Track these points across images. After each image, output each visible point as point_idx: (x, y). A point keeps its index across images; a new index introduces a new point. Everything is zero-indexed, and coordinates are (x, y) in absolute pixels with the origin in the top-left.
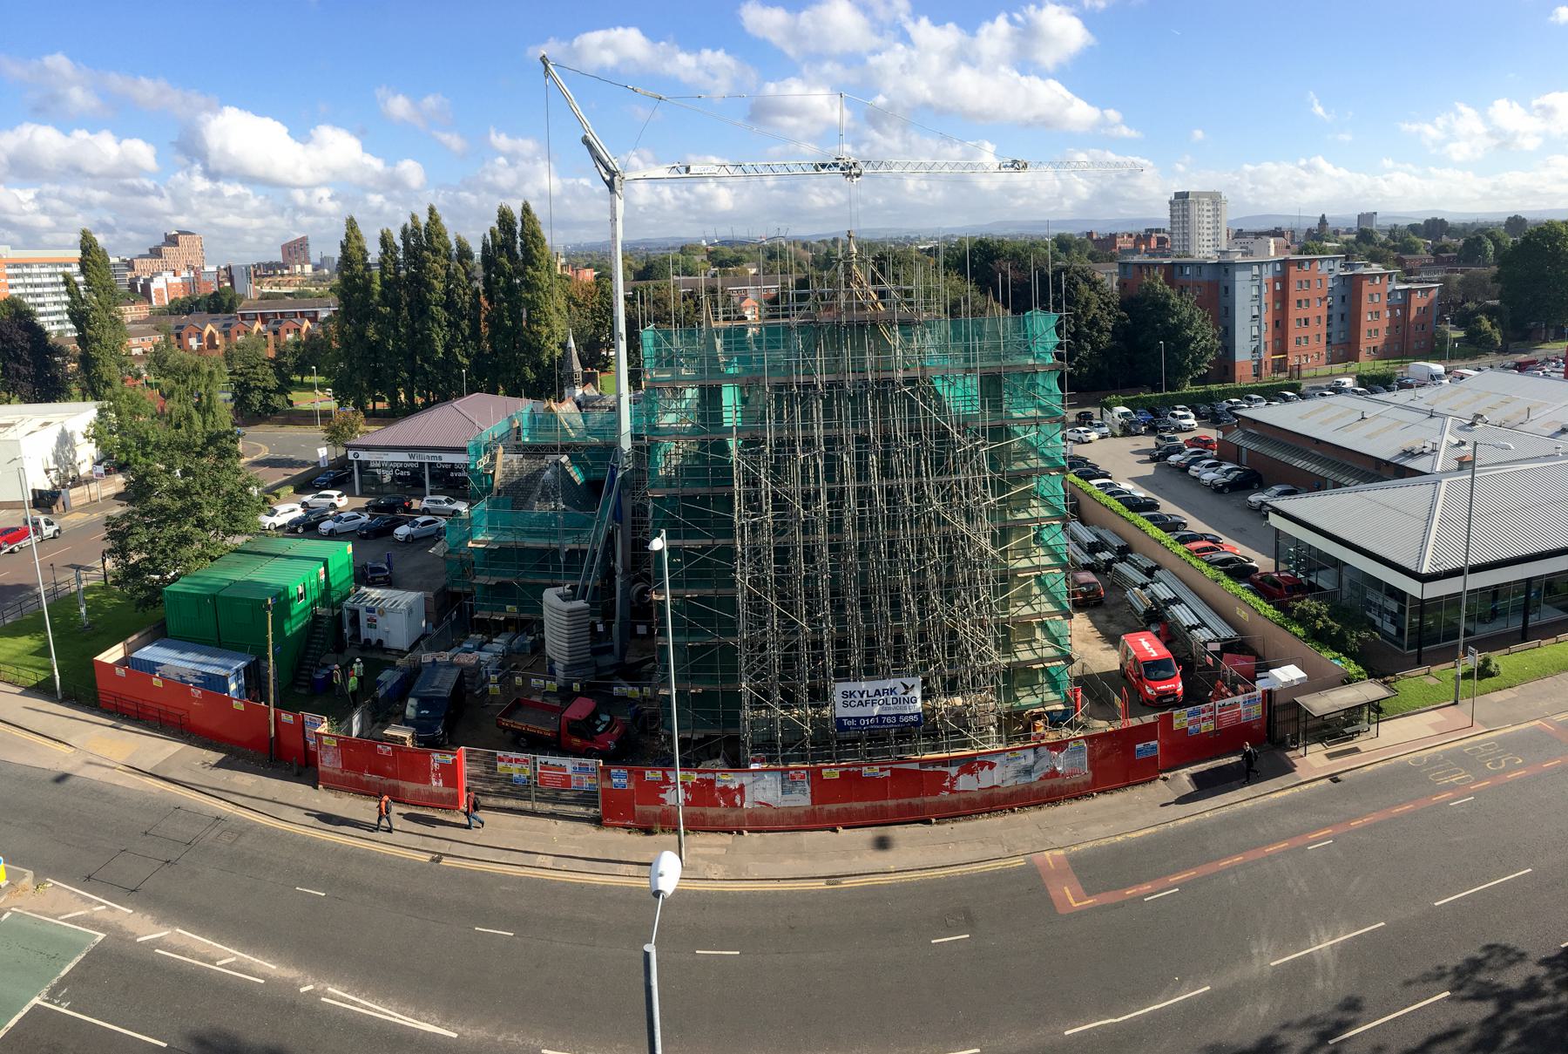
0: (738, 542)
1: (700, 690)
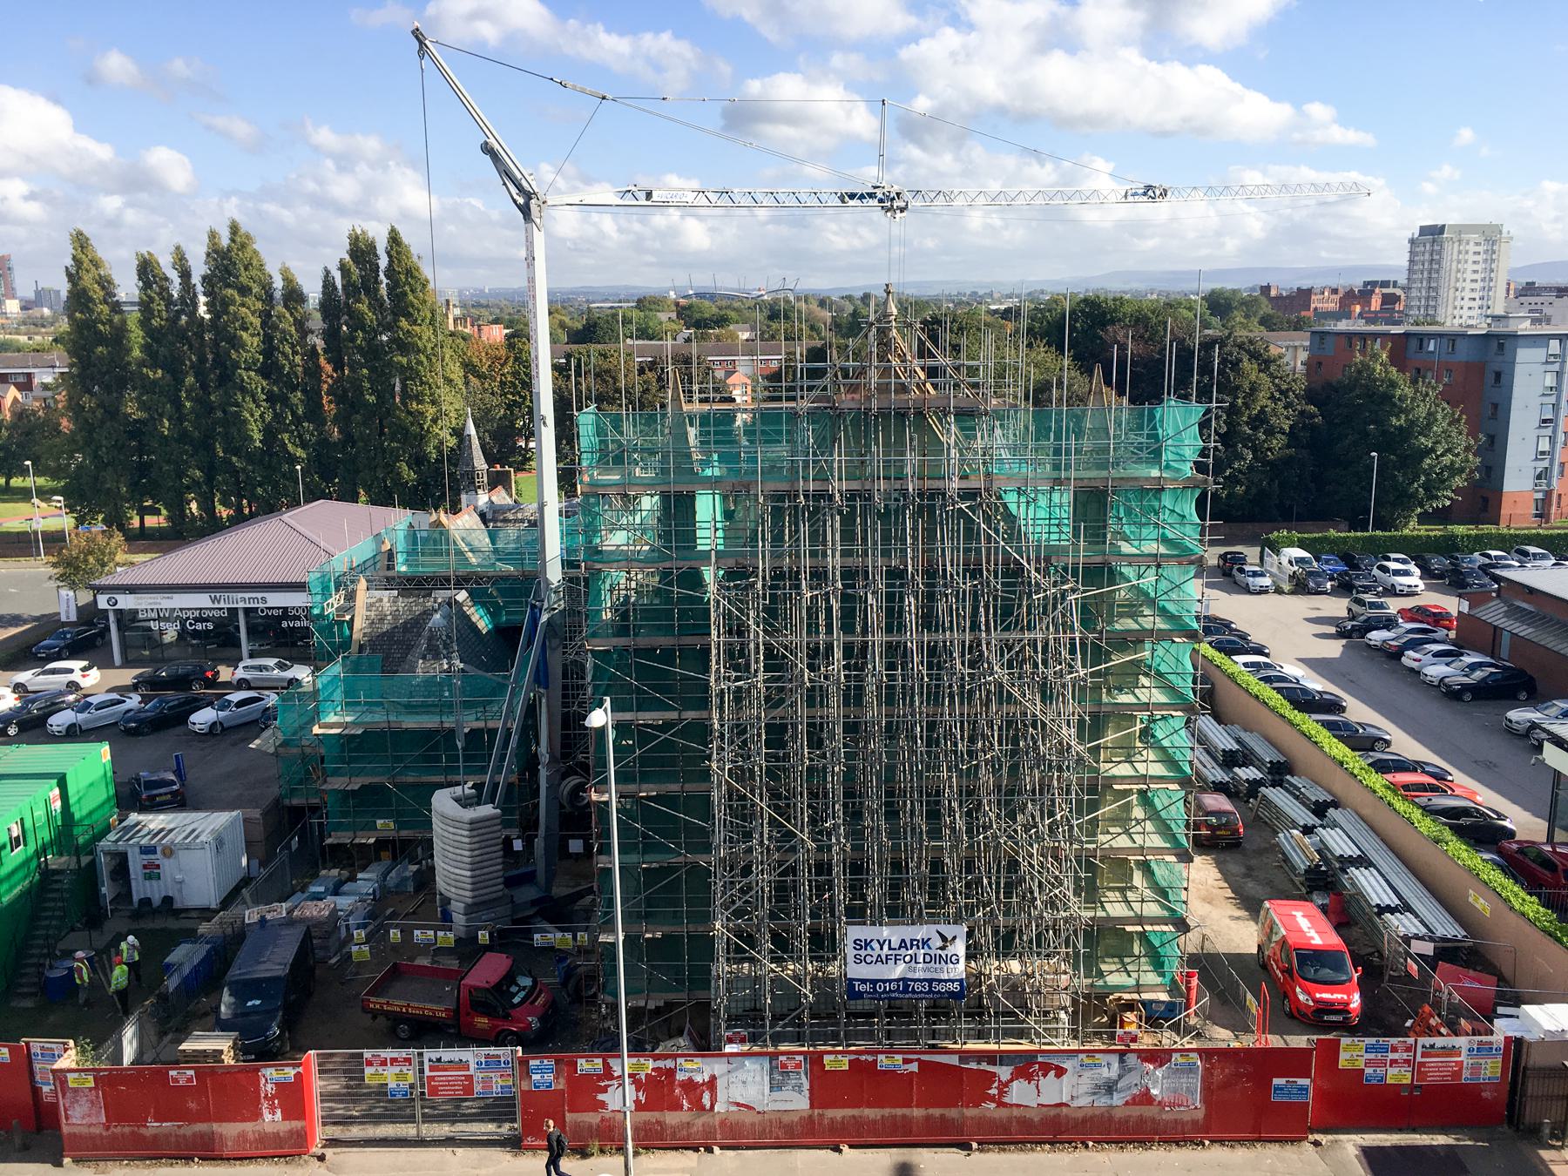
0: (715, 716)
1: (659, 935)
